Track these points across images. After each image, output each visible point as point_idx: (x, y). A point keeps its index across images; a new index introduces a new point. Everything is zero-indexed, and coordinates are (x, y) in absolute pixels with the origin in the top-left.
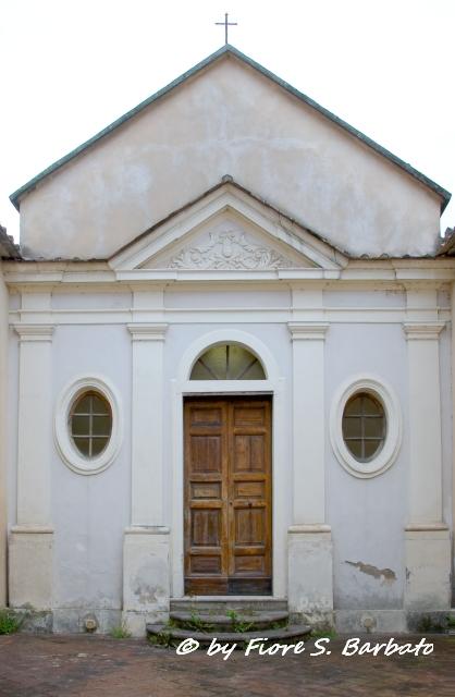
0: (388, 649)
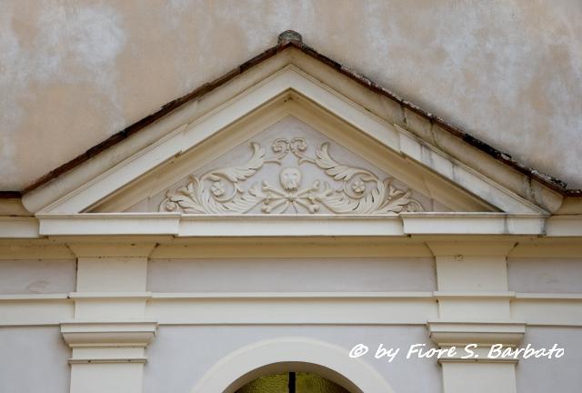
0: (526, 352)
